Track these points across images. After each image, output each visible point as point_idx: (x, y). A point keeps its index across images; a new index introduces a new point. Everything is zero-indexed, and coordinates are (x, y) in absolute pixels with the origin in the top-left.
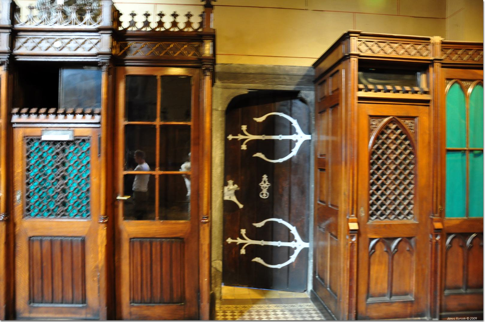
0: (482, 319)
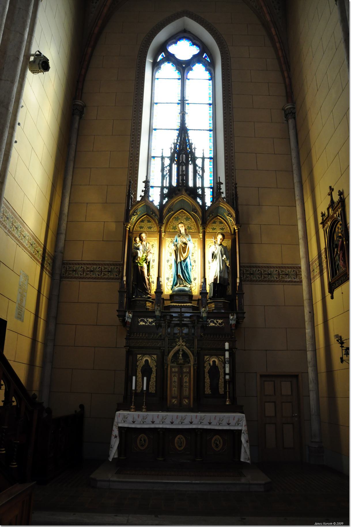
0: (348, 524)
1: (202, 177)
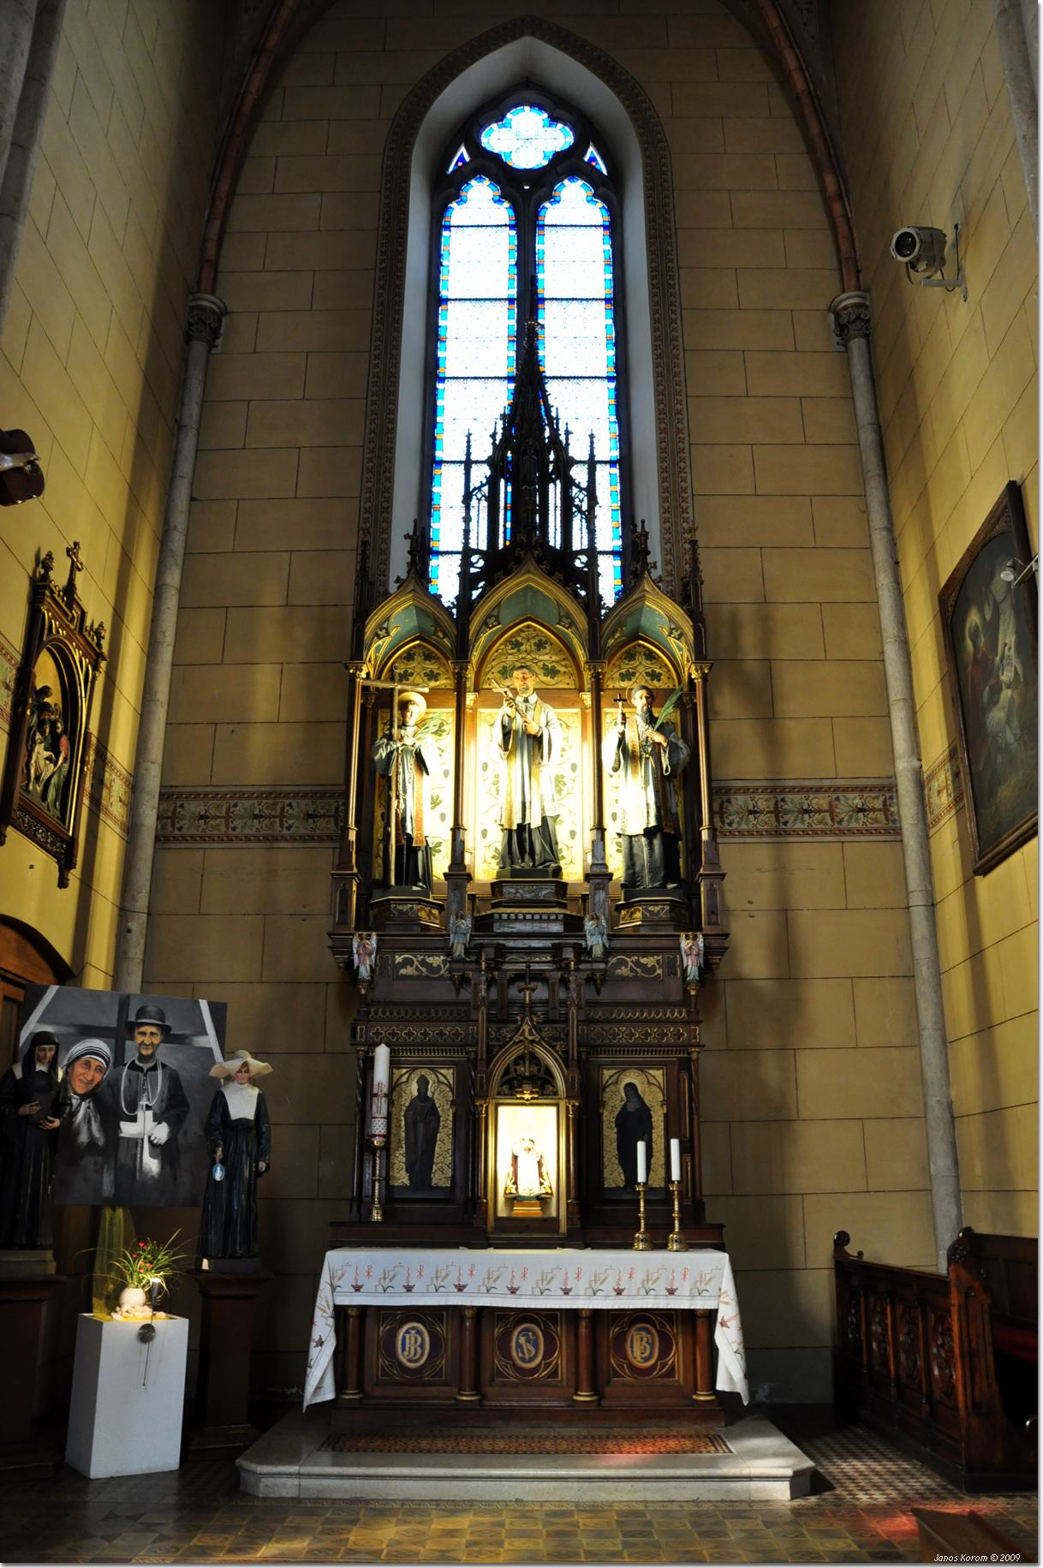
0: (1034, 1559)
1: (590, 517)
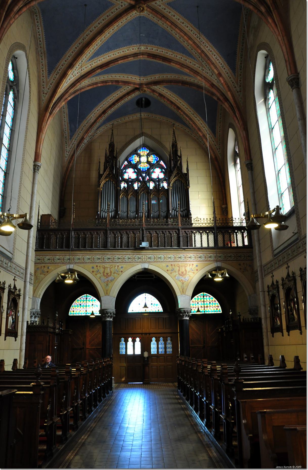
0: (305, 467)
